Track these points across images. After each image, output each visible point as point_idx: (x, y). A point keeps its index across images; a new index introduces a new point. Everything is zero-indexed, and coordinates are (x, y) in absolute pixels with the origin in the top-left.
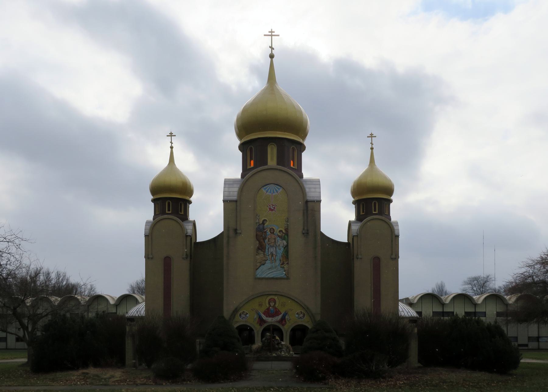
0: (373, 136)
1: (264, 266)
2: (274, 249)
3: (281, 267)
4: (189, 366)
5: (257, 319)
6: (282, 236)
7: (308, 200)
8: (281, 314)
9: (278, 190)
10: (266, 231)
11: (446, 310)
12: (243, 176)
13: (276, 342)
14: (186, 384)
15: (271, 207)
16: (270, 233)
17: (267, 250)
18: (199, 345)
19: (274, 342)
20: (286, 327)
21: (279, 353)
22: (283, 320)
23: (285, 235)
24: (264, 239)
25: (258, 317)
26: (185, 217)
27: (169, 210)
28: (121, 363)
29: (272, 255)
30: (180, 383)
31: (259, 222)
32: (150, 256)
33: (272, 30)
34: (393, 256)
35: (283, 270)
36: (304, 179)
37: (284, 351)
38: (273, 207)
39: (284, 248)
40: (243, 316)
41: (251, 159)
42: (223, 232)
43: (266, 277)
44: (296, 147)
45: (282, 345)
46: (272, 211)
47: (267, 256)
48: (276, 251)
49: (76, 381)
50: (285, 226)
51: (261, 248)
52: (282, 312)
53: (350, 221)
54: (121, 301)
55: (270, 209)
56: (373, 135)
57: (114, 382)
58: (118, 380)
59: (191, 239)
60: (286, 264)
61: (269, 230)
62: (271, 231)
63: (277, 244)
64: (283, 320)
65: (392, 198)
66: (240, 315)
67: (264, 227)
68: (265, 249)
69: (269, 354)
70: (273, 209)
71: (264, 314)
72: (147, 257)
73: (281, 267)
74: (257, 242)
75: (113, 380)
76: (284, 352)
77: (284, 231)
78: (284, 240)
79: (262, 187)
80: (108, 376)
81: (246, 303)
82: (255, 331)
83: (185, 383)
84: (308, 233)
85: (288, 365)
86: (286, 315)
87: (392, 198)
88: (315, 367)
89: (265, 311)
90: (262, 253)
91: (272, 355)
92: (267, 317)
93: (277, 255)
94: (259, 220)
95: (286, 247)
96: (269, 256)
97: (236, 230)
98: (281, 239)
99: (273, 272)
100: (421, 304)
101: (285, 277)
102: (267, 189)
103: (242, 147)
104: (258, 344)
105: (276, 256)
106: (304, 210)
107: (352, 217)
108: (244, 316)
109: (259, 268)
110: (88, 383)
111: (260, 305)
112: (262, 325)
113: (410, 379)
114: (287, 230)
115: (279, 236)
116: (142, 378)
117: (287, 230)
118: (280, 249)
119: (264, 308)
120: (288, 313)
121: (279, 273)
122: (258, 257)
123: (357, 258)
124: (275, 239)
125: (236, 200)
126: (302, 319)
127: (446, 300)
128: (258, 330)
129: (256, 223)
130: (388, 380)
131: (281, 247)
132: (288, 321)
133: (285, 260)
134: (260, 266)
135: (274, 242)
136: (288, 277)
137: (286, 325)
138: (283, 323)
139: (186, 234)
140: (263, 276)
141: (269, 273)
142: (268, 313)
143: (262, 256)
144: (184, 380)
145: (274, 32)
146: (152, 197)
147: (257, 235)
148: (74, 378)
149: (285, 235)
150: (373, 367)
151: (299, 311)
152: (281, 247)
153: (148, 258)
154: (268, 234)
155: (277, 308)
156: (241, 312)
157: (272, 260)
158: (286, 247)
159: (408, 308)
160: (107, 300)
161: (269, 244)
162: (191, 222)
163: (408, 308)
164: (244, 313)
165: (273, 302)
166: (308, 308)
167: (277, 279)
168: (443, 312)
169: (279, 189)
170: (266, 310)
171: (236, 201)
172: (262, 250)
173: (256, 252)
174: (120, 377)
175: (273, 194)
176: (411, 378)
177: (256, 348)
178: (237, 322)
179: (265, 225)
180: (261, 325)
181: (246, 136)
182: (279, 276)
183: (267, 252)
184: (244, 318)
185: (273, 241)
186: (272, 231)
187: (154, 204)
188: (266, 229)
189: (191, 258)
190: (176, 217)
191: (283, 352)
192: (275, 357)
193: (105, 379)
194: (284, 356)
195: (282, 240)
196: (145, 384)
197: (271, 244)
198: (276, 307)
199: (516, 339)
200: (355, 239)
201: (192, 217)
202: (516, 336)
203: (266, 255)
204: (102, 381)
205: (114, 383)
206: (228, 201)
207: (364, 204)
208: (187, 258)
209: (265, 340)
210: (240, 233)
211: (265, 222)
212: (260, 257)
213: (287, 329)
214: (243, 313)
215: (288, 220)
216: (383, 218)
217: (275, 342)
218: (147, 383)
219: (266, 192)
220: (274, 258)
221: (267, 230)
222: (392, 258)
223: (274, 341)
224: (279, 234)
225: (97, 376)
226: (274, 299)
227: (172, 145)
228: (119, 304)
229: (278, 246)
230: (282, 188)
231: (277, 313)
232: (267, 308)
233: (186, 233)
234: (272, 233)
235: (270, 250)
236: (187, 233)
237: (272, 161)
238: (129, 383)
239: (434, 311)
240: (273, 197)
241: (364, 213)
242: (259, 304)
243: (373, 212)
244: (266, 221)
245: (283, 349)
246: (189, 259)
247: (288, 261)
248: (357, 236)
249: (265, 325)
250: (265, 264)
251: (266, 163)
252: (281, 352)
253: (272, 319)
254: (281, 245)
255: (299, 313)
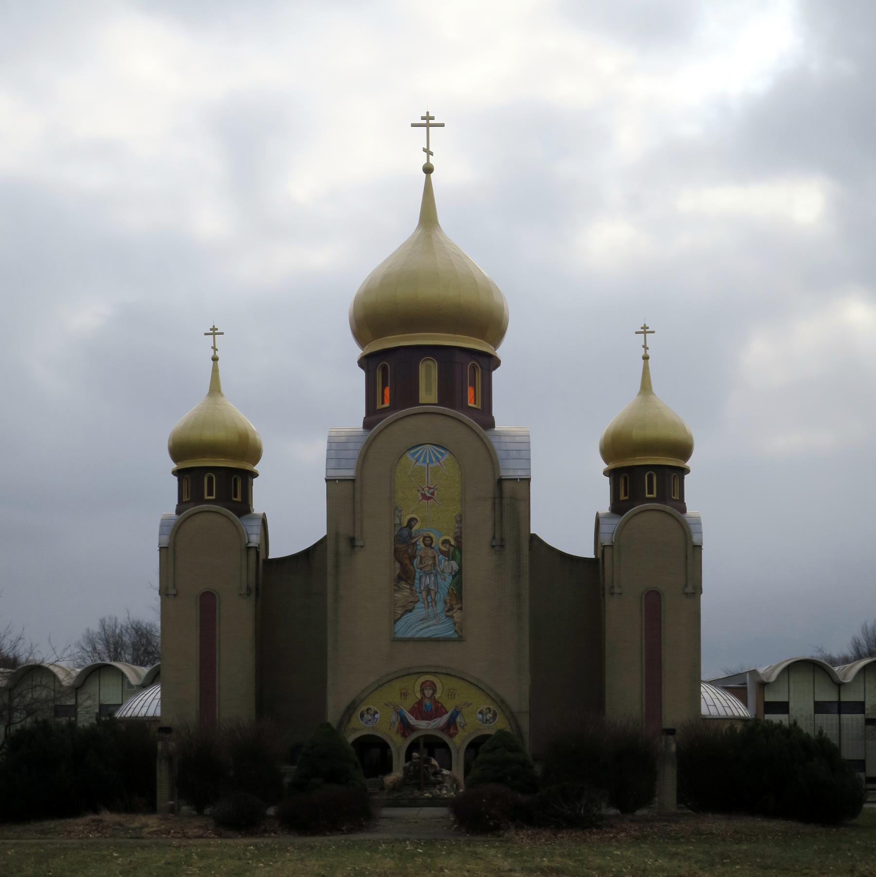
0: (647, 330)
1: (411, 614)
2: (433, 578)
3: (447, 616)
4: (271, 811)
5: (397, 724)
6: (449, 551)
7: (502, 478)
8: (447, 712)
9: (440, 457)
10: (416, 542)
11: (847, 697)
12: (368, 425)
13: (432, 771)
14: (269, 837)
15: (426, 492)
16: (423, 546)
17: (416, 581)
18: (289, 772)
19: (428, 770)
20: (457, 740)
21: (438, 791)
22: (451, 726)
23: (456, 550)
24: (412, 557)
25: (399, 719)
26: (244, 508)
27: (210, 494)
28: (151, 808)
29: (429, 591)
30: (258, 835)
31: (400, 524)
32: (172, 591)
33: (428, 113)
34: (689, 590)
35: (452, 622)
36: (496, 429)
37: (446, 787)
38: (431, 491)
39: (454, 577)
40: (367, 717)
41: (384, 385)
42: (325, 538)
43: (415, 637)
44: (479, 363)
45: (443, 776)
46: (428, 500)
47: (418, 595)
48: (436, 584)
49: (85, 832)
50: (457, 530)
51: (405, 576)
52: (447, 710)
53: (597, 513)
54: (86, 679)
55: (424, 497)
56: (648, 328)
57: (149, 833)
58: (156, 831)
59: (258, 553)
60: (458, 609)
61: (421, 539)
62: (426, 542)
63: (439, 569)
64: (451, 726)
65: (689, 464)
66: (362, 715)
67: (410, 534)
68: (414, 578)
69: (417, 793)
70: (430, 495)
71: (412, 712)
72: (164, 592)
73: (447, 616)
74: (398, 565)
75: (146, 830)
76: (446, 790)
77: (453, 543)
78: (452, 560)
79: (406, 451)
80: (136, 824)
81: (374, 690)
82: (393, 749)
83: (267, 835)
84: (502, 546)
85: (441, 811)
86: (457, 716)
87: (689, 464)
88: (483, 809)
89: (413, 707)
90: (408, 587)
91: (423, 795)
92: (417, 718)
93: (439, 590)
94: (400, 519)
95: (458, 575)
96: (421, 593)
97: (352, 541)
98: (447, 558)
99: (429, 626)
100: (787, 684)
101: (456, 636)
102: (417, 455)
103: (365, 362)
104: (396, 775)
105: (436, 593)
106: (494, 498)
107: (604, 505)
108: (370, 718)
109: (400, 618)
110: (107, 835)
111: (404, 695)
112: (407, 734)
113: (645, 829)
114: (458, 539)
115: (442, 552)
116: (195, 828)
117: (460, 539)
118: (445, 580)
119: (411, 702)
120: (461, 711)
121: (441, 628)
122: (399, 596)
123: (612, 594)
124: (434, 558)
125: (354, 478)
126: (490, 723)
127: (845, 676)
128: (399, 745)
129: (395, 525)
130: (606, 830)
131: (447, 575)
132: (461, 727)
133: (454, 602)
134: (402, 615)
135: (431, 565)
136: (460, 637)
137: (457, 735)
138: (451, 733)
139: (247, 544)
140: (409, 635)
141: (422, 629)
142: (419, 711)
143: (406, 593)
144: (265, 831)
145: (433, 118)
146: (174, 466)
147: (396, 550)
148: (81, 828)
149: (456, 550)
150: (580, 809)
151: (484, 707)
152: (447, 575)
153: (167, 595)
154: (418, 548)
155: (438, 702)
156: (363, 708)
157: (428, 601)
158: (458, 575)
159: (725, 698)
160: (54, 676)
161: (421, 569)
162: (255, 517)
163: (725, 698)
164: (369, 712)
165: (430, 689)
166: (503, 701)
167: (438, 640)
168: (839, 703)
169: (442, 454)
170: (416, 706)
171: (353, 480)
172: (406, 581)
173: (395, 585)
174: (159, 826)
175: (431, 465)
176: (646, 828)
177: (391, 782)
178: (355, 730)
179: (414, 529)
180: (404, 735)
181: (374, 342)
182: (442, 635)
183: (418, 585)
184: (370, 720)
185: (430, 562)
186: (429, 542)
187: (179, 480)
188: (415, 538)
189: (257, 595)
190: (224, 507)
191: (444, 789)
192: (428, 798)
193: (134, 829)
194: (446, 796)
195: (449, 560)
196: (201, 837)
197: (426, 569)
198: (436, 698)
199: (861, 764)
200: (608, 552)
201: (260, 503)
202: (861, 758)
203: (416, 592)
204: (130, 833)
205: (149, 836)
206: (336, 480)
207: (628, 478)
208: (248, 595)
209: (410, 766)
210: (362, 547)
211: (413, 523)
212: (404, 595)
213: (458, 743)
214: (367, 713)
215: (461, 520)
216: (668, 508)
217: (429, 770)
218: (205, 835)
219: (414, 462)
220: (433, 598)
221: (418, 540)
222: (686, 594)
223: (426, 768)
224: (443, 548)
225: (121, 825)
226: (432, 682)
227: (215, 353)
228: (83, 684)
229: (441, 573)
230: (448, 453)
231: (439, 710)
232: (417, 700)
233: (247, 541)
234: (428, 546)
235: (423, 580)
236: (249, 542)
237: (428, 393)
238: (175, 835)
239: (817, 700)
240: (429, 472)
241: (627, 498)
242: (401, 693)
243: (647, 496)
244: (415, 521)
245: (445, 785)
246: (253, 596)
247: (462, 603)
248: (612, 546)
249: (414, 736)
250: (414, 611)
251: (415, 402)
252: (440, 790)
253: (429, 724)
254: (447, 570)
255: (485, 712)
